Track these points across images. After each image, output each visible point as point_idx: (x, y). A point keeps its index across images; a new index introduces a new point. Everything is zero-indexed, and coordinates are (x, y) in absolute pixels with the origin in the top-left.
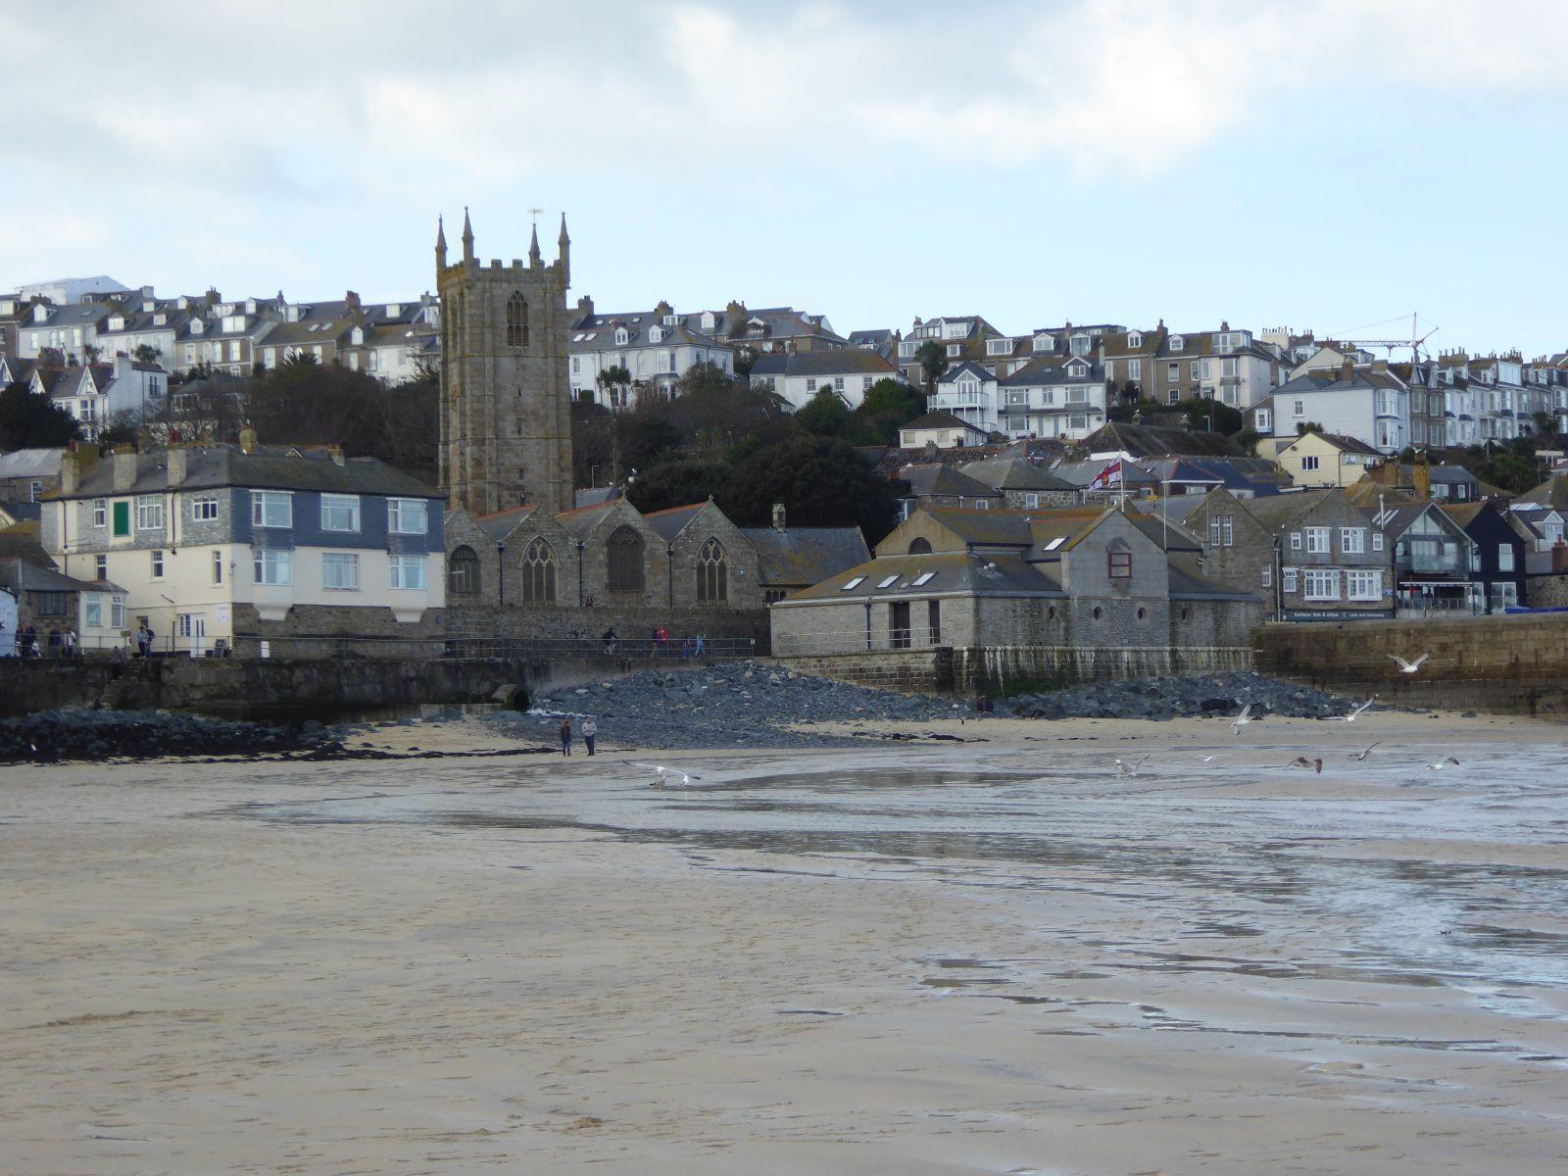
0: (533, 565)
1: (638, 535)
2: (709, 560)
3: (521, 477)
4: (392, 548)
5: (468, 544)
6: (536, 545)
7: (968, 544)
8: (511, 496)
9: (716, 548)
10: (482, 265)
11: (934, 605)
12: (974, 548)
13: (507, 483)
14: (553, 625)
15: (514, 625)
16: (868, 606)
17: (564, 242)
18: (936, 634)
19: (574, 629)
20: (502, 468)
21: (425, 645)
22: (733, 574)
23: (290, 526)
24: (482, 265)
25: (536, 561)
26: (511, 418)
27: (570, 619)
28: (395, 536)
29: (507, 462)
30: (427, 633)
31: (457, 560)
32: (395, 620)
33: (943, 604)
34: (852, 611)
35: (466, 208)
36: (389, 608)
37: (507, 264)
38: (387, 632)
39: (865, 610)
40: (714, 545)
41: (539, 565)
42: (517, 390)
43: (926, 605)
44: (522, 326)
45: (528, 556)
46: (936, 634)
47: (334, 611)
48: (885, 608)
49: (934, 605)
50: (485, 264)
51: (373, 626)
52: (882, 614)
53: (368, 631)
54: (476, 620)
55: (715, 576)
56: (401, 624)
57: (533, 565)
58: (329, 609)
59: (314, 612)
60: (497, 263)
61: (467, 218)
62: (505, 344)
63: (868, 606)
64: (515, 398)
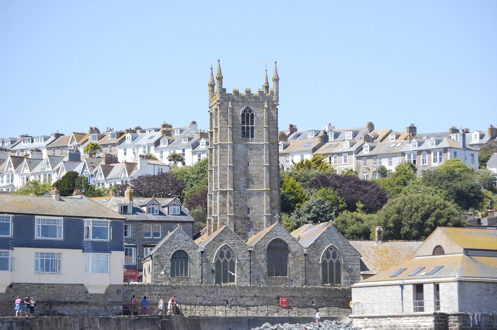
0: (222, 261)
1: (286, 244)
2: (330, 259)
3: (249, 213)
4: (86, 248)
5: (183, 249)
6: (223, 250)
7: (465, 249)
8: (242, 223)
9: (334, 252)
10: (227, 92)
11: (437, 287)
12: (469, 251)
13: (240, 216)
14: (212, 296)
15: (185, 295)
16: (402, 286)
18: (437, 304)
19: (225, 299)
20: (237, 207)
21: (108, 307)
22: (344, 267)
23: (62, 238)
24: (227, 92)
25: (230, 259)
26: (243, 179)
27: (223, 292)
28: (87, 242)
29: (240, 204)
30: (110, 300)
31: (176, 258)
32: (87, 292)
33: (441, 286)
34: (393, 289)
35: (219, 61)
36: (83, 285)
37: (242, 92)
38: (82, 299)
39: (400, 288)
40: (333, 250)
41: (225, 261)
43: (432, 286)
44: (250, 126)
45: (219, 256)
46: (437, 304)
47: (42, 287)
48: (411, 288)
49: (437, 287)
50: (229, 91)
51: (71, 295)
52: (409, 291)
53: (67, 299)
54: (159, 292)
55: (333, 268)
56: (91, 295)
57: (222, 261)
58: (39, 285)
59: (28, 288)
60: (236, 92)
62: (240, 137)
63: (402, 286)
64: (245, 167)
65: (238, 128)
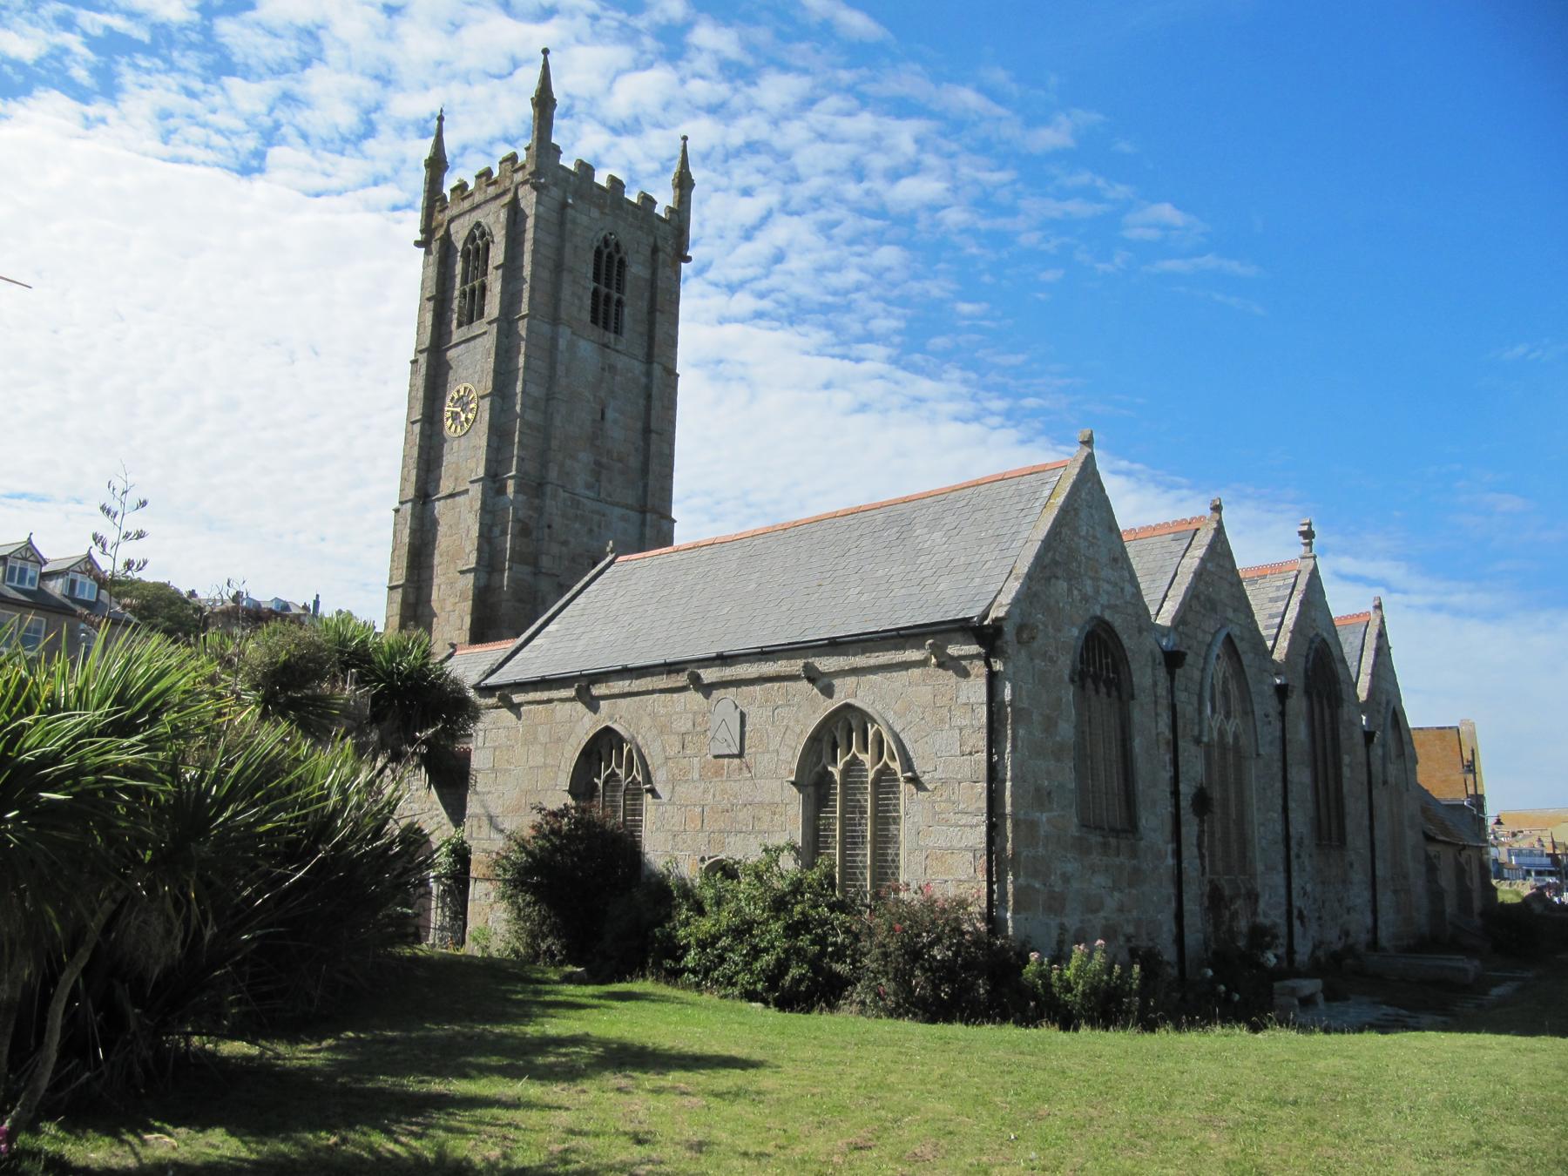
17: (684, 183)
42: (598, 408)
44: (615, 296)
61: (546, 67)
64: (594, 421)
65: (585, 288)
